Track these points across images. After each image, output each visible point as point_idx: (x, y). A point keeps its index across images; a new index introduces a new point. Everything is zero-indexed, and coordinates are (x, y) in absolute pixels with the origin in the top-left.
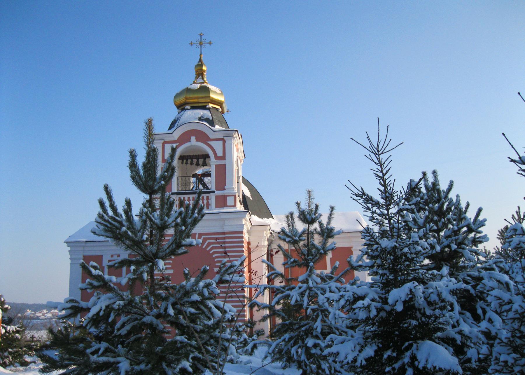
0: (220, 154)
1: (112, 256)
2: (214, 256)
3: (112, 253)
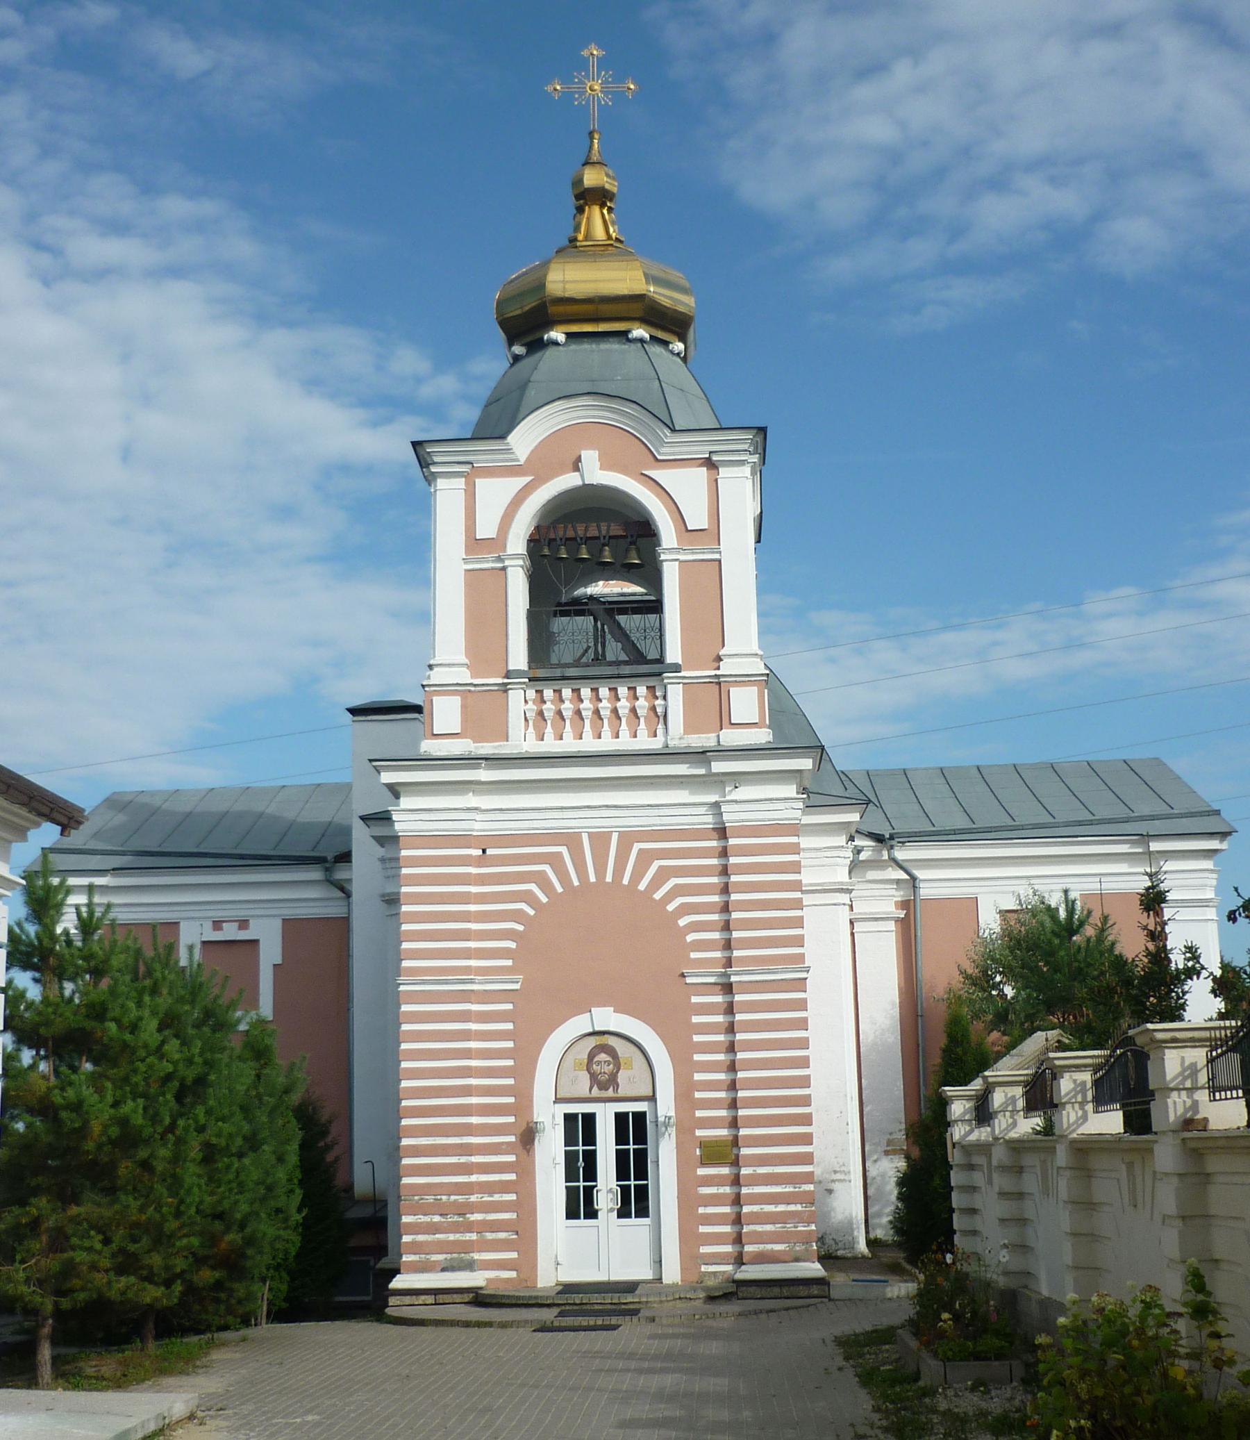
0: (697, 518)
1: (217, 925)
2: (682, 922)
3: (218, 914)
